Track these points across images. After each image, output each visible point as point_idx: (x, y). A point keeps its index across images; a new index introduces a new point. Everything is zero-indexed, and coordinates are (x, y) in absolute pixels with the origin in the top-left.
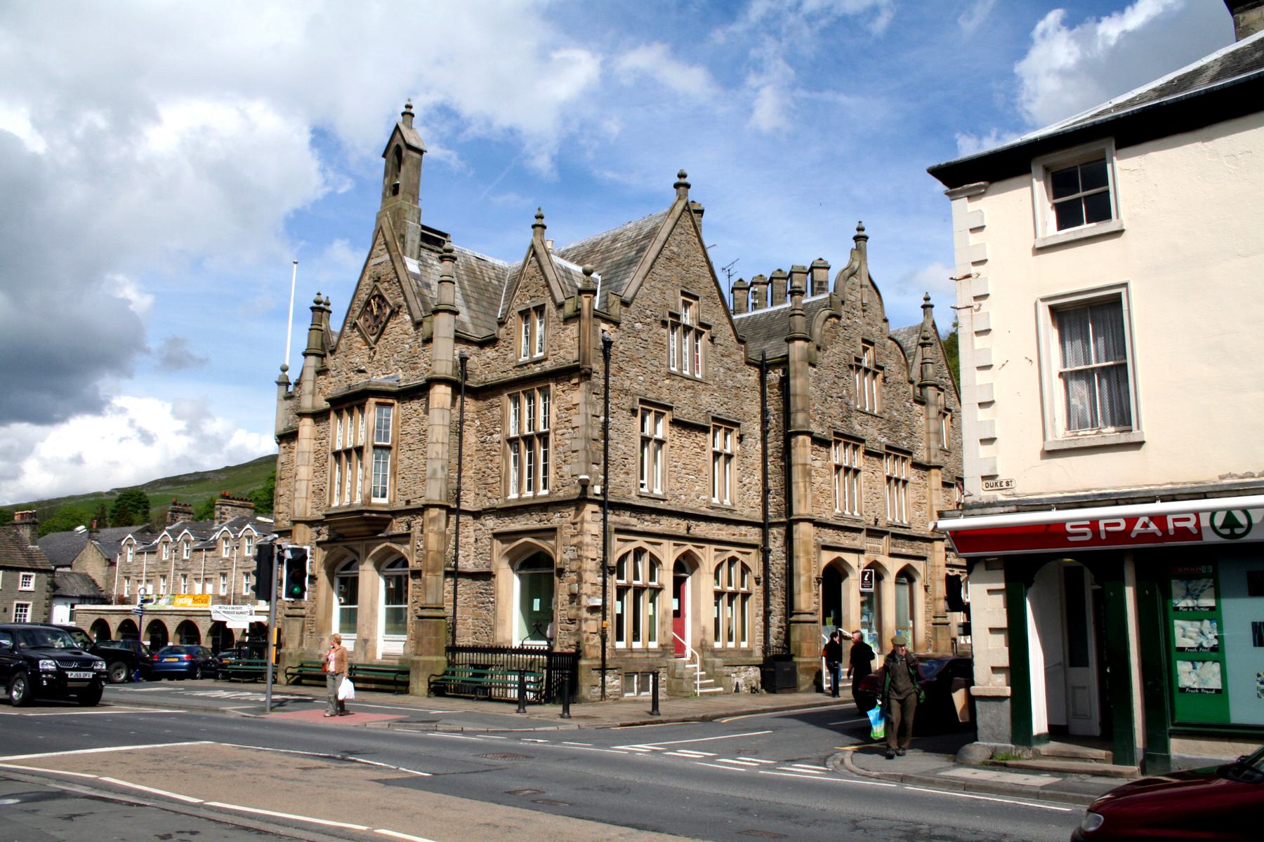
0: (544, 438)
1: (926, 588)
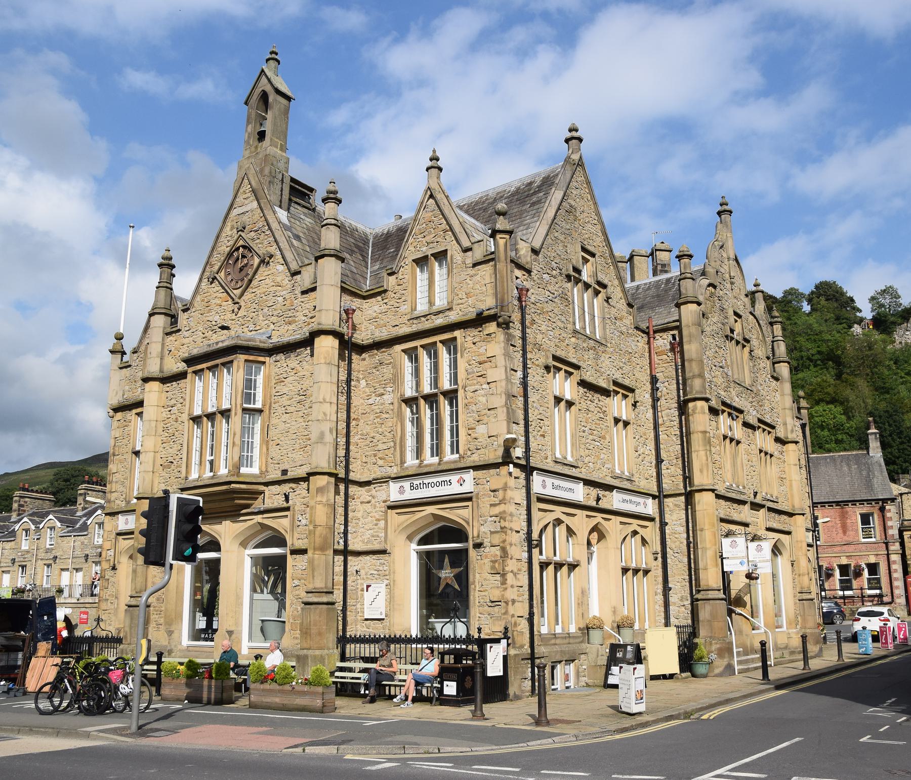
0: (451, 395)
1: (809, 561)
